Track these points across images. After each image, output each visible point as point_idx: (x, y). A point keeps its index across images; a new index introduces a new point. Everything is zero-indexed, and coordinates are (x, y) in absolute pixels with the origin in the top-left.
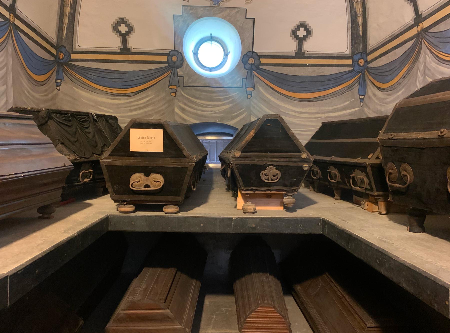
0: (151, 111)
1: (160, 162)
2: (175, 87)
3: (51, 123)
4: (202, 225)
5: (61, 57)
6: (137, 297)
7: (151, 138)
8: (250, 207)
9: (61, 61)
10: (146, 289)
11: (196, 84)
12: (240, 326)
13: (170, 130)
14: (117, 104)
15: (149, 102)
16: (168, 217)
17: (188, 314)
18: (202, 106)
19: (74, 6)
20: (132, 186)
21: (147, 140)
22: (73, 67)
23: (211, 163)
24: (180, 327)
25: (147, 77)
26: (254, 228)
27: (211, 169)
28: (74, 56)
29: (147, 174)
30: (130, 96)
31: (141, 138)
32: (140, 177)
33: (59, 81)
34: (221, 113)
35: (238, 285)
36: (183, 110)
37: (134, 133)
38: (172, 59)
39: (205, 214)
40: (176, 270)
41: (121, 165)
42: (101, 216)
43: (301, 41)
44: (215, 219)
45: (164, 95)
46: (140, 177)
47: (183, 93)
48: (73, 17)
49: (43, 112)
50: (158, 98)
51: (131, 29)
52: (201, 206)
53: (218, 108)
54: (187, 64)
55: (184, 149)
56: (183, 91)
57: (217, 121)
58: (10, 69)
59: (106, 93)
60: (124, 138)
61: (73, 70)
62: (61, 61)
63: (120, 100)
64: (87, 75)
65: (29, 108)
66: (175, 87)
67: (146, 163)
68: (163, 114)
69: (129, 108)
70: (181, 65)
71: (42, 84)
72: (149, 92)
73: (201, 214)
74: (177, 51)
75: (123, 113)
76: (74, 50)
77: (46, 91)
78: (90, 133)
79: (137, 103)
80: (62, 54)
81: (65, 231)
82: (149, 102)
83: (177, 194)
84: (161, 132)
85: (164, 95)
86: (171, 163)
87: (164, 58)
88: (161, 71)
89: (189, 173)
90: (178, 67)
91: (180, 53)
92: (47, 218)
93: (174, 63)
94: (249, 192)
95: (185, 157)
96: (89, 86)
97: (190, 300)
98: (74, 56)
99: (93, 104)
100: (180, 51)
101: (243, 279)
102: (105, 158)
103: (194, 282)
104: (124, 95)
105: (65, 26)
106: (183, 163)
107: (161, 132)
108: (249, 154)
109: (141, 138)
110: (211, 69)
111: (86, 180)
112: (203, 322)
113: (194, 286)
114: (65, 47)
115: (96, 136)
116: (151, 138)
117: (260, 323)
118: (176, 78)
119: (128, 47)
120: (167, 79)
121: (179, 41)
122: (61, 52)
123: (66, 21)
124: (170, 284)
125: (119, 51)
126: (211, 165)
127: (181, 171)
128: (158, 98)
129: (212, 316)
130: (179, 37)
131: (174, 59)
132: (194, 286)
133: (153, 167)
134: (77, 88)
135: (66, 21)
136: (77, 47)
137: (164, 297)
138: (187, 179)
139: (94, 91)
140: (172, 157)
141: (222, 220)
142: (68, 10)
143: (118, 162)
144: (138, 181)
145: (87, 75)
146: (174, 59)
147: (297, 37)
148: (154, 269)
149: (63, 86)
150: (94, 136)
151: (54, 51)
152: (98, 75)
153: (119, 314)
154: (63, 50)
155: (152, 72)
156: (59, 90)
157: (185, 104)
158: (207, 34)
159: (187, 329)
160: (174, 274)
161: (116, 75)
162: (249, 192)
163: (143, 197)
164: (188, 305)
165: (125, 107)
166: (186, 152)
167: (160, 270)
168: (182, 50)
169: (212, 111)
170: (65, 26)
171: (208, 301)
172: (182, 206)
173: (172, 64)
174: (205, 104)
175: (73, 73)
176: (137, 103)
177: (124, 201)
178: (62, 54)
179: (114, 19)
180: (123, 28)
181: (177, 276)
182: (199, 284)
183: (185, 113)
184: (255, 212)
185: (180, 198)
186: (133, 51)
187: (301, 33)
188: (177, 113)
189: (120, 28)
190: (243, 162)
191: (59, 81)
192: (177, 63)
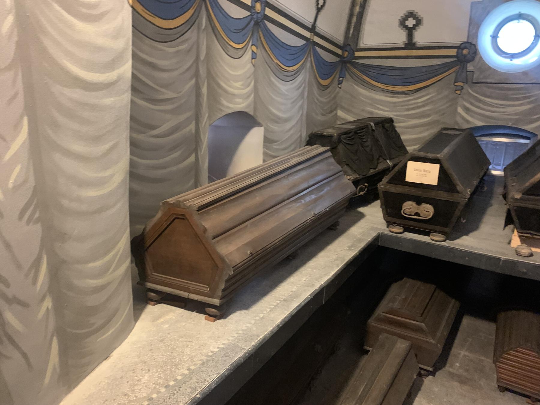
0: (430, 110)
1: (433, 194)
2: (461, 84)
3: (341, 148)
4: (467, 258)
5: (346, 56)
6: (396, 305)
7: (426, 171)
8: (525, 250)
9: (345, 59)
10: (405, 300)
11: (489, 81)
12: (495, 359)
13: (446, 165)
14: (395, 103)
15: (429, 101)
16: (434, 245)
17: (443, 331)
18: (492, 106)
19: (363, 6)
20: (404, 212)
21: (422, 173)
22: (355, 65)
23: (495, 169)
24: (433, 341)
25: (431, 72)
26: (526, 273)
27: (494, 176)
28: (357, 54)
29: (419, 203)
30: (409, 94)
31: (417, 170)
32: (412, 205)
33: (341, 79)
34: (516, 114)
35: (502, 316)
36: (467, 110)
37: (411, 165)
38: (462, 52)
39: (472, 247)
40: (435, 287)
41: (396, 192)
42: (374, 234)
43: (410, 32)
44: (482, 256)
45: (446, 93)
46: (412, 205)
47: (470, 91)
48: (361, 15)
49: (335, 137)
50: (440, 96)
51: (419, 22)
52: (471, 235)
53: (514, 108)
54: (481, 58)
55: (458, 185)
56: (471, 88)
57: (510, 124)
58: (307, 84)
59: (384, 91)
60: (402, 169)
61: (355, 67)
62: (345, 59)
63: (398, 97)
64: (367, 72)
65: (325, 134)
66: (461, 84)
67: (420, 193)
68: (443, 114)
69: (406, 107)
70: (472, 59)
71: (327, 87)
72: (430, 90)
73: (467, 246)
74: (471, 43)
75: (399, 112)
76: (358, 48)
77: (330, 92)
78: (367, 147)
79: (416, 101)
80: (347, 53)
81: (350, 248)
82: (429, 101)
83: (446, 225)
84: (437, 167)
85: (446, 93)
86: (443, 196)
87: (453, 52)
88: (446, 67)
89: (460, 208)
90: (468, 61)
91: (474, 45)
92: (333, 229)
93: (465, 56)
94: (526, 235)
95: (458, 192)
96: (368, 83)
97: (446, 317)
98: (357, 54)
99: (370, 102)
100: (474, 43)
101: (510, 313)
102: (383, 185)
103: (453, 301)
104: (403, 93)
105: (353, 25)
106: (455, 198)
107: (437, 167)
108: (532, 197)
109: (417, 170)
110: (513, 56)
111: (362, 193)
112: (457, 342)
113: (453, 305)
114: (349, 45)
115: (373, 149)
116: (426, 171)
117: (519, 363)
118: (464, 74)
119: (414, 42)
120: (454, 75)
121: (474, 31)
122: (346, 51)
123: (354, 19)
124: (427, 301)
125: (403, 46)
126: (494, 172)
127: (453, 205)
128: (440, 96)
129: (468, 339)
130: (475, 25)
131: (465, 52)
132: (453, 305)
133: (425, 198)
134: (357, 85)
135: (354, 19)
136: (361, 45)
137: (422, 312)
138: (457, 213)
139: (373, 88)
140: (445, 191)
141: (490, 258)
142: (357, 9)
143: (394, 189)
144: (409, 207)
145: (367, 72)
146: (465, 52)
147: (406, 27)
148: (415, 282)
149: (345, 84)
150: (371, 150)
151: (339, 52)
152: (379, 72)
153: (379, 315)
154: (348, 48)
155: (437, 67)
156: (340, 88)
157: (472, 104)
158: (516, 12)
159: (439, 345)
160: (433, 290)
161: (397, 72)
162: (526, 235)
163: (412, 223)
164: (444, 323)
165: (402, 106)
166: (460, 188)
167: (419, 283)
168: (477, 41)
169: (508, 111)
170: (353, 25)
171: (467, 321)
172: (449, 237)
173: (465, 55)
174: (496, 104)
175: (355, 70)
176: (416, 101)
177: (395, 223)
178: (347, 53)
179: (402, 13)
180: (410, 22)
181: (435, 294)
182: (458, 304)
183: (469, 115)
184: (531, 255)
185: (447, 230)
186: (418, 45)
187: (410, 22)
188: (460, 114)
189: (407, 23)
190: (522, 205)
191: (341, 79)
192: (469, 57)
